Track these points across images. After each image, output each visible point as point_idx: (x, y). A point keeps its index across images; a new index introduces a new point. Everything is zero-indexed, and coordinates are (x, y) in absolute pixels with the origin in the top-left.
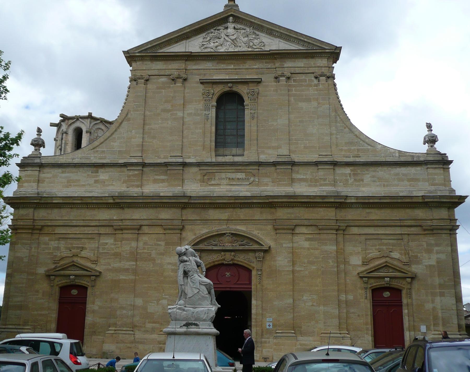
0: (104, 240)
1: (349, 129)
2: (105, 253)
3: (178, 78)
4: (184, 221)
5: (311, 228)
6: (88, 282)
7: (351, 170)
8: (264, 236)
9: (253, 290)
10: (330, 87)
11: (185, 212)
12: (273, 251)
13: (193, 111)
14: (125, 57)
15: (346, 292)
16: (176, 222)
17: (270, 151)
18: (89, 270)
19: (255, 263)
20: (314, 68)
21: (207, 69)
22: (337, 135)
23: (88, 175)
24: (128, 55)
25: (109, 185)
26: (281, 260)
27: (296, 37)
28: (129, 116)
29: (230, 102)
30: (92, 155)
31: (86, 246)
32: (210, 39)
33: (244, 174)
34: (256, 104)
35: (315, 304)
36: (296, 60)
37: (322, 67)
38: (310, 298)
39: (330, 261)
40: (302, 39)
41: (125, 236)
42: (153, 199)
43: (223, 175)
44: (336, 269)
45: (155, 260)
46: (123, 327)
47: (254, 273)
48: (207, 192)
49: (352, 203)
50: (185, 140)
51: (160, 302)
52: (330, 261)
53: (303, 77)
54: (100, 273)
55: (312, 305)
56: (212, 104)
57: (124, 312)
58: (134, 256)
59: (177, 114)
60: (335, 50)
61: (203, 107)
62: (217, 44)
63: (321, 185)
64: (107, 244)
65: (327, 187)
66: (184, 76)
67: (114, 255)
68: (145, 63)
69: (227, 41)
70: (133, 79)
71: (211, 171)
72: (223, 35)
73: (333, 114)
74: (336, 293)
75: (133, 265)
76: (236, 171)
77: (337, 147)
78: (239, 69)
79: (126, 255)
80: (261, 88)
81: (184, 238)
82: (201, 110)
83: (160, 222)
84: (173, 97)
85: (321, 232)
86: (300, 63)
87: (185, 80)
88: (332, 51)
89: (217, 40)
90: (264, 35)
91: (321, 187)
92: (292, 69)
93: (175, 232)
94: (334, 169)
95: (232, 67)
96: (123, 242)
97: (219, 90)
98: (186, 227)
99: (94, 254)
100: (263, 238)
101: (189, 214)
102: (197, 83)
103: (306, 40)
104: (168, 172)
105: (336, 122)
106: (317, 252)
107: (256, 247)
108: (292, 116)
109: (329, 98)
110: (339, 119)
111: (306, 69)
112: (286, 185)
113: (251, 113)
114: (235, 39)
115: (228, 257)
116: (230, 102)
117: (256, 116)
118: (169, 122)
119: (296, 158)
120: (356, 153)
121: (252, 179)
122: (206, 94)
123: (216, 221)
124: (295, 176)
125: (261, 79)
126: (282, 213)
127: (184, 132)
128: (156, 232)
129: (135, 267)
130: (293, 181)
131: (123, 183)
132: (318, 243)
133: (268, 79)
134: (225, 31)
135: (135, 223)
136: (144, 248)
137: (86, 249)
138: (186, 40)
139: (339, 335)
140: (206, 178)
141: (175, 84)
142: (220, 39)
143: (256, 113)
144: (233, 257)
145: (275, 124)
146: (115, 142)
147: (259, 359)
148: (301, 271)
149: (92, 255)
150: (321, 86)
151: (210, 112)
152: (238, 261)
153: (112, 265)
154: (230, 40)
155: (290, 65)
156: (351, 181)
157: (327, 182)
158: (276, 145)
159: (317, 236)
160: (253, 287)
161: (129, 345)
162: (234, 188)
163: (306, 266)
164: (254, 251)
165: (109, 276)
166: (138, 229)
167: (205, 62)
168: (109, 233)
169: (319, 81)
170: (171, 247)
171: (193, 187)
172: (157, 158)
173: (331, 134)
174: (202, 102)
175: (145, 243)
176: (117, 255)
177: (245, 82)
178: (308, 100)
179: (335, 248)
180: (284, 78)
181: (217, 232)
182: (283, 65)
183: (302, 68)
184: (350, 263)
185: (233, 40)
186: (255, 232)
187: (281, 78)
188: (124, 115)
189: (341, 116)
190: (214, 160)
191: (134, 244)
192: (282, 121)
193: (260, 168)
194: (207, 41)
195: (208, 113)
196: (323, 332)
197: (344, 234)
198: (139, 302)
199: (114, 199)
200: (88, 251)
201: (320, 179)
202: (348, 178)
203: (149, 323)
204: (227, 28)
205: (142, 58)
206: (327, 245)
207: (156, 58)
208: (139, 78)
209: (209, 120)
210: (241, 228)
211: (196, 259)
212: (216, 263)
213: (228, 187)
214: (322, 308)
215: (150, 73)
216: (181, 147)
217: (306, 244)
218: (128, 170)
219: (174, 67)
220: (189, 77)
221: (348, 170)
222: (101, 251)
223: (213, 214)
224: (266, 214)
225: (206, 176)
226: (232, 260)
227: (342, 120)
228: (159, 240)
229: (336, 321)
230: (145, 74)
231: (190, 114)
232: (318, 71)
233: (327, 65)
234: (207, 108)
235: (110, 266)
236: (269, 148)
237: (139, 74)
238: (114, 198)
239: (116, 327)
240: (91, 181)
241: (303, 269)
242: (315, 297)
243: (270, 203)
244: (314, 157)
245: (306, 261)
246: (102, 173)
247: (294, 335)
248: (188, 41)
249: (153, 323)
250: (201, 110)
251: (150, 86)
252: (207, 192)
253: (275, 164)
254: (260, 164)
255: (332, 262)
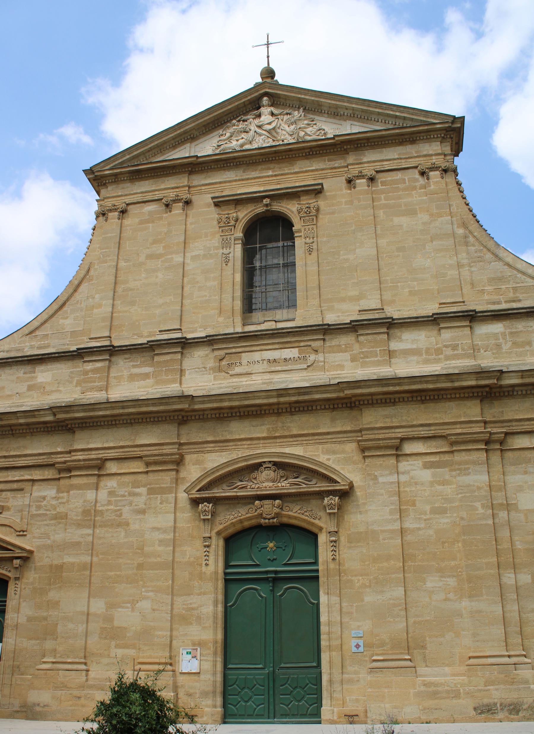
0: (39, 491)
1: (493, 253)
2: (39, 515)
3: (175, 201)
4: (184, 447)
5: (433, 443)
6: (10, 571)
7: (504, 326)
8: (339, 460)
9: (320, 574)
10: (450, 187)
11: (184, 429)
12: (358, 493)
13: (201, 252)
14: (89, 179)
15: (515, 567)
16: (167, 450)
17: (345, 306)
18: (9, 547)
19: (323, 519)
20: (417, 159)
21: (225, 182)
22: (471, 267)
23: (18, 378)
24: (91, 176)
25: (52, 391)
26: (372, 512)
27: (380, 111)
28: (92, 273)
29: (267, 232)
30: (28, 344)
31: (9, 504)
32: (231, 136)
33: (297, 349)
34: (315, 227)
35: (451, 596)
36: (384, 149)
37: (431, 155)
38: (441, 584)
39: (478, 505)
40: (391, 113)
41: (75, 481)
42: (123, 408)
43: (257, 356)
44: (490, 522)
45: (128, 524)
46: (68, 657)
47: (322, 539)
48: (226, 387)
49: (513, 386)
50: (186, 302)
51: (137, 606)
52: (478, 505)
53: (399, 175)
54: (31, 552)
55: (447, 599)
56: (235, 235)
57: (71, 626)
58: (91, 517)
59: (172, 258)
60: (453, 123)
61: (219, 242)
62: (241, 141)
63: (447, 358)
64: (44, 498)
65: (460, 361)
66: (185, 196)
67: (56, 518)
68: (121, 186)
69: (260, 135)
70: (102, 214)
71: (234, 350)
72: (253, 128)
73: (461, 231)
74: (494, 571)
75: (89, 535)
76: (281, 346)
77: (473, 288)
78: (282, 175)
79: (77, 515)
80: (322, 203)
81: (184, 478)
82: (217, 248)
83: (138, 452)
84: (166, 234)
85: (454, 448)
86: (391, 155)
87: (188, 203)
88: (447, 125)
89: (243, 135)
90: (323, 119)
91: (448, 362)
92: (376, 164)
93: (165, 468)
94: (471, 327)
95: (270, 173)
96: (71, 492)
97: (245, 214)
98: (188, 458)
99: (22, 519)
100: (337, 468)
101: (193, 433)
102: (208, 205)
103: (397, 114)
104: (156, 359)
105: (467, 244)
106: (448, 490)
107: (324, 486)
108: (382, 242)
109: (450, 206)
110: (471, 239)
111: (403, 161)
112: (378, 364)
113: (306, 243)
114: (274, 129)
115: (269, 508)
116: (267, 232)
117: (315, 246)
118: (160, 275)
119: (394, 312)
120: (511, 295)
121: (312, 357)
122: (225, 225)
123: (244, 443)
124: (394, 345)
125: (322, 184)
126: (372, 418)
127: (185, 289)
128: (133, 470)
129: (91, 538)
130: (391, 354)
131: (76, 386)
132: (451, 470)
133: (334, 185)
134: (257, 121)
135: (93, 455)
136: (109, 503)
137: (8, 509)
138: (191, 143)
139: (506, 660)
140: (224, 363)
141: (170, 211)
142: (247, 132)
143: (315, 243)
144: (277, 510)
145: (351, 257)
146: (67, 318)
147: (339, 717)
148: (419, 529)
149: (18, 521)
150: (432, 187)
151: (232, 249)
152: (289, 517)
153: (52, 537)
154: (264, 132)
155: (372, 158)
156: (505, 348)
157: (460, 351)
158: (357, 293)
159: (447, 457)
160: (321, 567)
161: (76, 693)
162: (277, 377)
163: (428, 519)
164: (321, 495)
165: (42, 559)
166: (97, 467)
167: (222, 172)
168: (49, 477)
169: (428, 179)
170: (159, 496)
171: (200, 378)
172: (136, 337)
173: (459, 266)
174: (218, 236)
175: (111, 493)
176: (61, 518)
177: (293, 195)
178: (411, 212)
179: (485, 478)
180: (365, 180)
181: (246, 460)
182: (361, 159)
183: (395, 161)
184: (520, 507)
185: (269, 132)
186: (323, 458)
187: (358, 181)
188: (83, 273)
189: (475, 234)
190: (239, 329)
191: (90, 495)
192: (365, 250)
193: (327, 337)
194: (225, 140)
195: (228, 251)
196: (471, 654)
197: (502, 450)
198: (98, 606)
199: (55, 415)
200: (12, 511)
201: (446, 346)
202: (501, 340)
203: (117, 646)
204: (259, 116)
205: (116, 179)
206: (469, 474)
207: (137, 175)
208: (110, 211)
209: (230, 264)
210: (295, 451)
211: (50, 512)
212: (247, 524)
213: (267, 376)
214: (465, 603)
215: (128, 200)
216: (179, 313)
217: (426, 475)
218: (85, 362)
219: (168, 187)
220: (194, 198)
221: (497, 328)
222: (35, 512)
223: (238, 429)
224: (343, 423)
225: (224, 360)
226: (277, 515)
227: (477, 239)
228: (136, 485)
229: (498, 631)
230: (120, 203)
231: (194, 258)
232: (425, 163)
233: (440, 152)
234: (225, 244)
235: (49, 539)
236: (343, 300)
237: (109, 203)
238: (54, 410)
239: (55, 657)
240: (23, 388)
241: (422, 526)
242: (452, 582)
243: (347, 400)
244: (430, 308)
245: (428, 508)
246: (42, 372)
247: (408, 663)
248: (193, 144)
249: (124, 648)
250: (217, 248)
251: (128, 221)
252: (226, 387)
253: (354, 327)
254: (326, 330)
255: (483, 506)
